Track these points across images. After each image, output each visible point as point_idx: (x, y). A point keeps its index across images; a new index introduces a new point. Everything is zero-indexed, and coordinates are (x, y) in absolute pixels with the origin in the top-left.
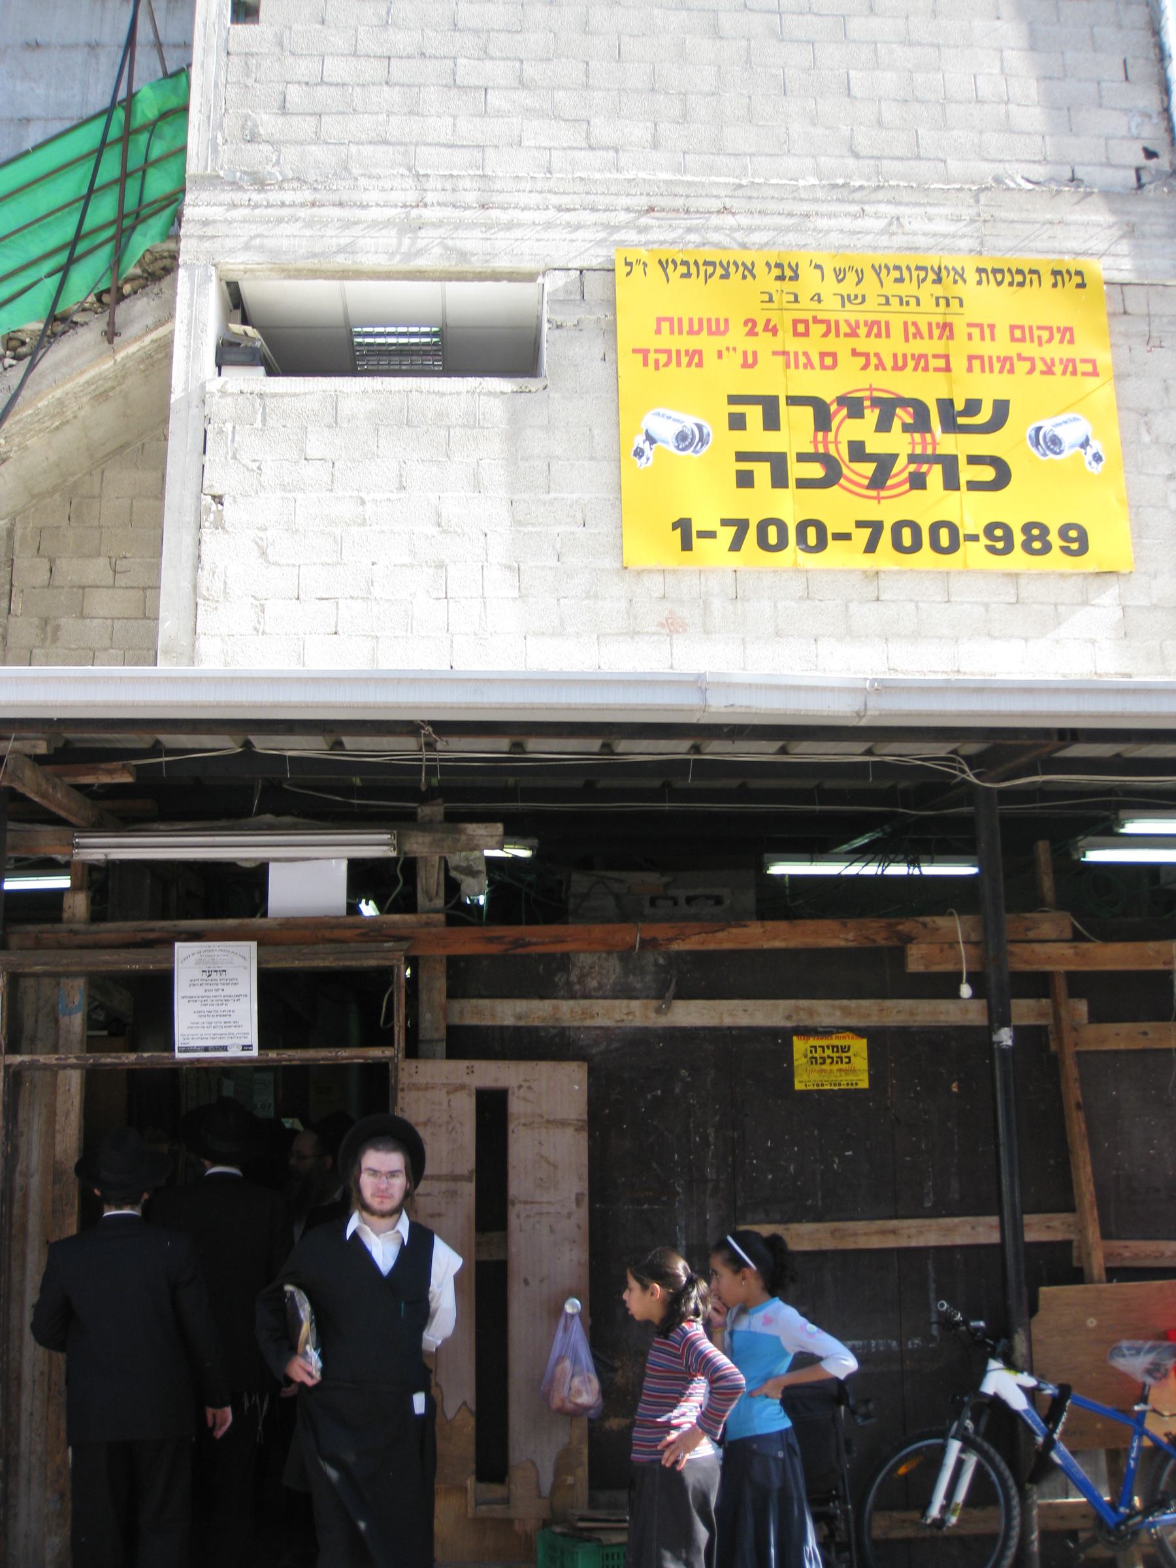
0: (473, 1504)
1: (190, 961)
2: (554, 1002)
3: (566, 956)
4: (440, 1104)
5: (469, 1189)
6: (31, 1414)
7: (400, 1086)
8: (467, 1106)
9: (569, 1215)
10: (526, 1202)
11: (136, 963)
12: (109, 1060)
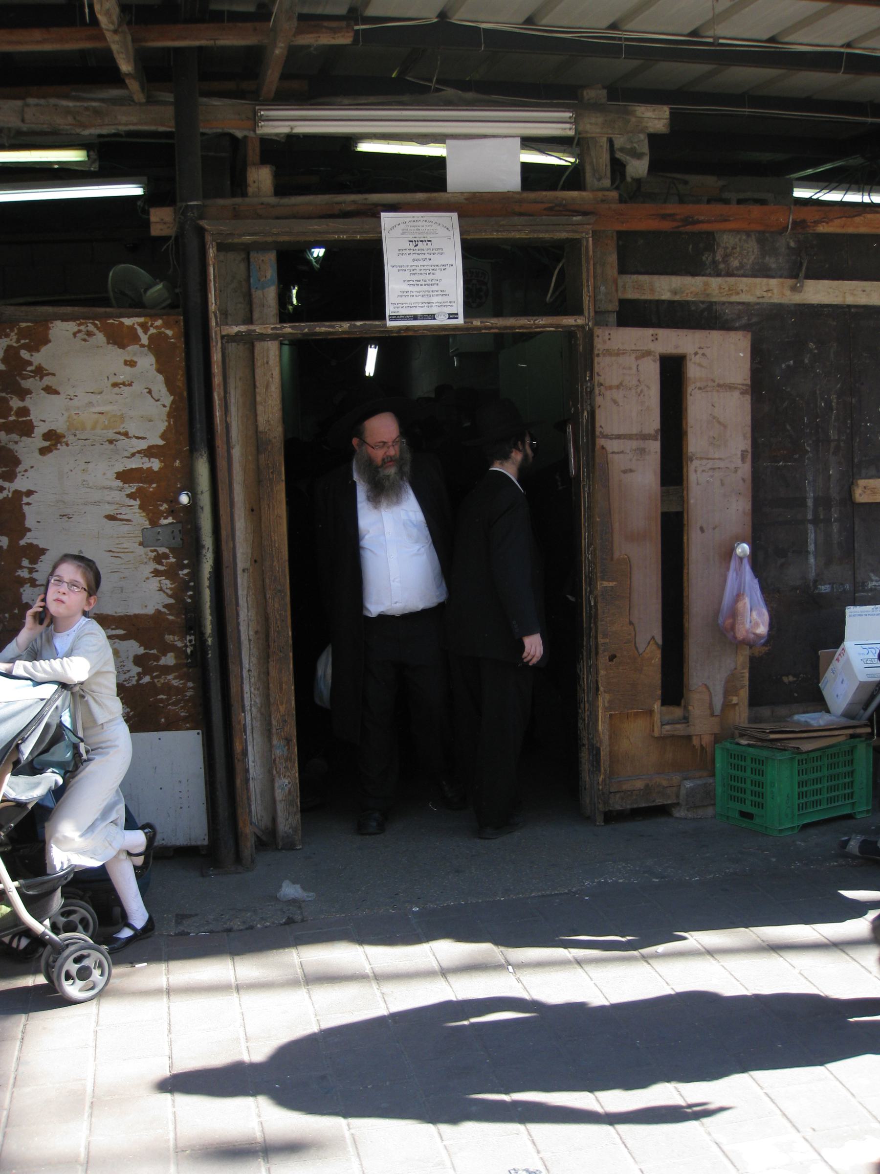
0: (659, 724)
1: (397, 231)
2: (704, 278)
3: (711, 235)
4: (630, 368)
5: (655, 446)
6: (249, 670)
7: (596, 352)
8: (652, 371)
9: (736, 470)
10: (701, 459)
11: (343, 233)
12: (323, 329)
